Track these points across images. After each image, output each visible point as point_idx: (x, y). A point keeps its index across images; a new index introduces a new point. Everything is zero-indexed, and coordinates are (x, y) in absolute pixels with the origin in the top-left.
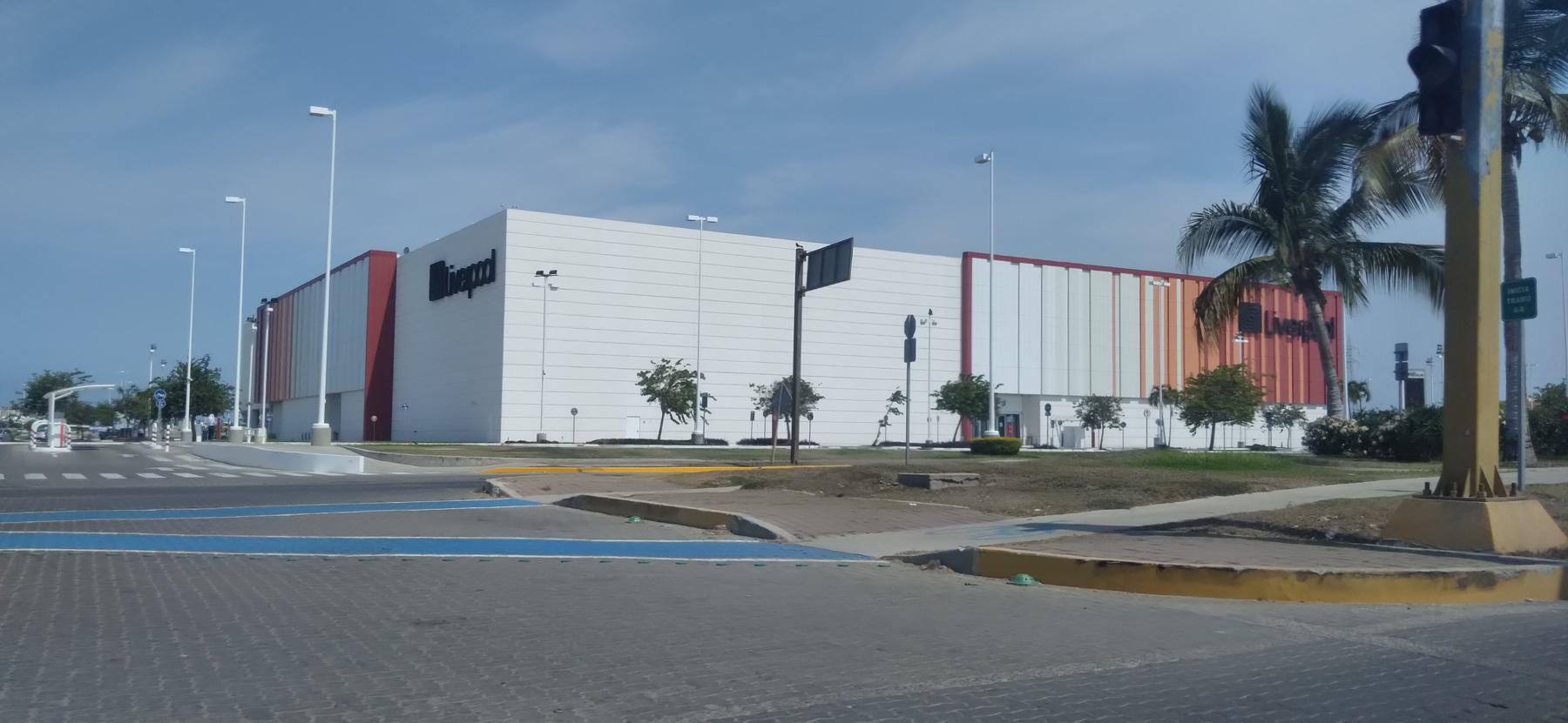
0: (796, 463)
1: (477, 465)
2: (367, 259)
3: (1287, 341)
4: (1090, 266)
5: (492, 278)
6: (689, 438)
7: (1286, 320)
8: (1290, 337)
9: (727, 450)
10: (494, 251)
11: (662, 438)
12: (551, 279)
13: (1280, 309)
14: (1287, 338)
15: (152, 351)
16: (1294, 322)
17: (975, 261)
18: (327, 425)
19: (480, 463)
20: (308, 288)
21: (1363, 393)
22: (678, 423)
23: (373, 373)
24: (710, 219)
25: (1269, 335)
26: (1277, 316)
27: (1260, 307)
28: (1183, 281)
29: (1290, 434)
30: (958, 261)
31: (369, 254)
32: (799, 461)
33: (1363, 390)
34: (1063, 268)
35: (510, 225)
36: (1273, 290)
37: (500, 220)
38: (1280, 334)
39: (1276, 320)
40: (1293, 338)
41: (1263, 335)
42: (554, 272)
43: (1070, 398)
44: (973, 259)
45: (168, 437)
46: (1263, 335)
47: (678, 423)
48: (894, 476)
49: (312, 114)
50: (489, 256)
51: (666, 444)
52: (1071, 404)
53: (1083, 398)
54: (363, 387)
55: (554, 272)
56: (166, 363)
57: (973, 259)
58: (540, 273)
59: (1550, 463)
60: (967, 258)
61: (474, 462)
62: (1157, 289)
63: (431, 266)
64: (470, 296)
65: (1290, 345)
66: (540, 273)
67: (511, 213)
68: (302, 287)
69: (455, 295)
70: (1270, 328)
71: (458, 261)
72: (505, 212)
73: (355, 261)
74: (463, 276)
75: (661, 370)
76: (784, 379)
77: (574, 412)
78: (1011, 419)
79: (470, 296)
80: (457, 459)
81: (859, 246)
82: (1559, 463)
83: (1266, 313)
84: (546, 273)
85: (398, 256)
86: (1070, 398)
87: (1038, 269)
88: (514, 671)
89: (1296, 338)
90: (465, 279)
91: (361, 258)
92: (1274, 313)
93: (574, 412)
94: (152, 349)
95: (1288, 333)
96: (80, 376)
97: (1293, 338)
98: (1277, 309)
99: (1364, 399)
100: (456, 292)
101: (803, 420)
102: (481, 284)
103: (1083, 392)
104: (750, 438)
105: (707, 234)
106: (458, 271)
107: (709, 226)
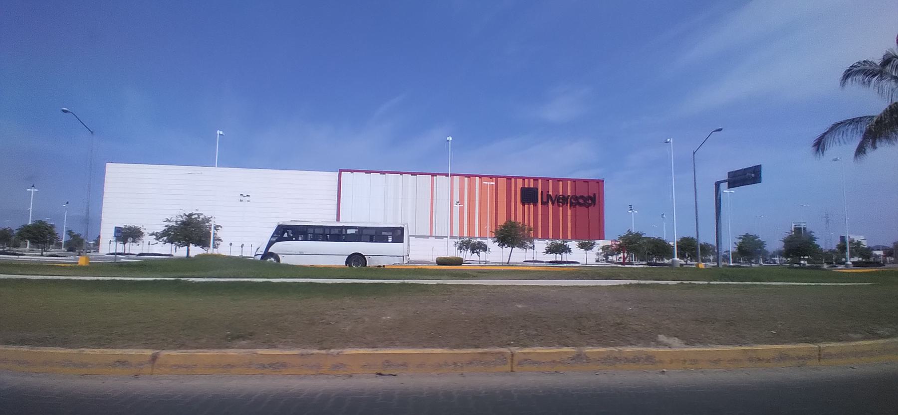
60: (341, 171)
70: (545, 200)
77: (231, 244)
93: (231, 244)
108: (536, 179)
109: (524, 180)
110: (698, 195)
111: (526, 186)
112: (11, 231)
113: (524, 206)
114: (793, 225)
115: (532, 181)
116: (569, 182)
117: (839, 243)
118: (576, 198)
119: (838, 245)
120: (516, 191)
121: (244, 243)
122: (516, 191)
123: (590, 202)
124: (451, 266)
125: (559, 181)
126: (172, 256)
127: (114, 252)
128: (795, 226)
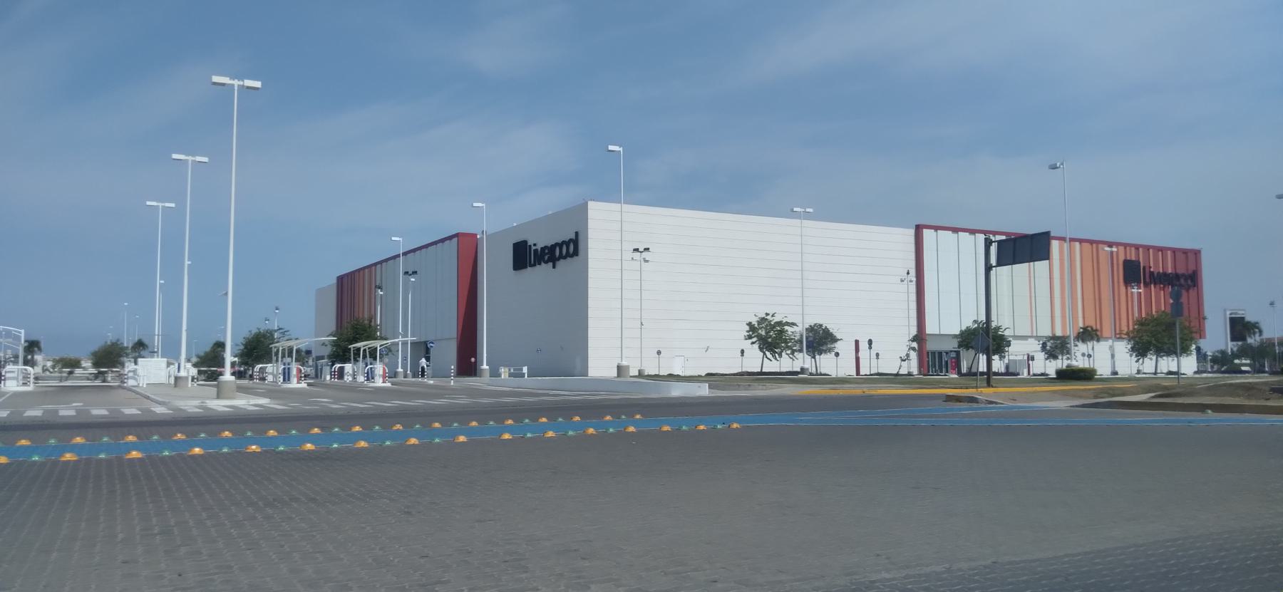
0: (992, 387)
1: (762, 390)
2: (455, 240)
3: (1160, 290)
4: (1093, 240)
5: (576, 253)
6: (637, 374)
7: (1159, 273)
8: (1162, 286)
9: (586, 379)
10: (577, 234)
11: (763, 371)
12: (645, 254)
13: (1154, 264)
14: (1160, 288)
15: (277, 311)
16: (1165, 274)
17: (926, 232)
18: (488, 367)
19: (764, 387)
20: (392, 261)
21: (1257, 330)
22: (771, 360)
23: (463, 326)
24: (808, 210)
25: (1146, 285)
26: (1152, 270)
27: (1139, 263)
28: (1080, 243)
29: (1178, 361)
30: (912, 232)
31: (457, 235)
32: (994, 385)
33: (1258, 328)
34: (933, 231)
35: (591, 213)
36: (1148, 250)
37: (583, 210)
38: (1155, 284)
39: (1152, 274)
40: (1164, 287)
41: (1142, 285)
42: (647, 249)
43: (1037, 338)
44: (924, 230)
45: (303, 375)
46: (1142, 285)
47: (771, 360)
48: (1267, 388)
49: (610, 151)
50: (573, 237)
51: (784, 375)
52: (1037, 342)
53: (1046, 337)
54: (456, 336)
55: (647, 249)
56: (268, 320)
57: (924, 230)
58: (637, 250)
59: (264, 416)
60: (919, 230)
61: (760, 387)
62: (1131, 256)
63: (514, 244)
64: (554, 267)
65: (1162, 292)
66: (637, 250)
67: (591, 204)
68: (386, 260)
69: (538, 266)
70: (1148, 280)
71: (540, 240)
72: (586, 204)
73: (443, 241)
74: (547, 251)
75: (763, 320)
76: (811, 326)
77: (659, 353)
78: (953, 355)
79: (554, 267)
80: (749, 385)
81: (1059, 243)
82: (701, 401)
83: (1144, 268)
84: (641, 250)
85: (478, 237)
86: (1037, 338)
87: (973, 237)
88: (396, 560)
89: (1167, 287)
90: (547, 254)
91: (450, 238)
92: (1150, 267)
93: (659, 353)
94: (277, 309)
95: (1161, 283)
96: (281, 331)
97: (1164, 287)
98: (1152, 265)
99: (1257, 335)
100: (540, 264)
101: (996, 357)
102: (565, 258)
103: (1046, 332)
104: (740, 371)
105: (807, 223)
106: (542, 248)
107: (807, 216)
108: (1137, 247)
109: (1125, 248)
110: (960, 254)
111: (1128, 258)
112: (1274, 339)
113: (1127, 288)
114: (1228, 313)
115: (1133, 249)
116: (1169, 252)
117: (1129, 346)
118: (1177, 276)
119: (1133, 349)
120: (1118, 265)
121: (660, 349)
122: (1118, 265)
123: (1189, 282)
124: (257, 403)
125: (1159, 250)
126: (1047, 375)
127: (876, 372)
128: (1231, 314)
